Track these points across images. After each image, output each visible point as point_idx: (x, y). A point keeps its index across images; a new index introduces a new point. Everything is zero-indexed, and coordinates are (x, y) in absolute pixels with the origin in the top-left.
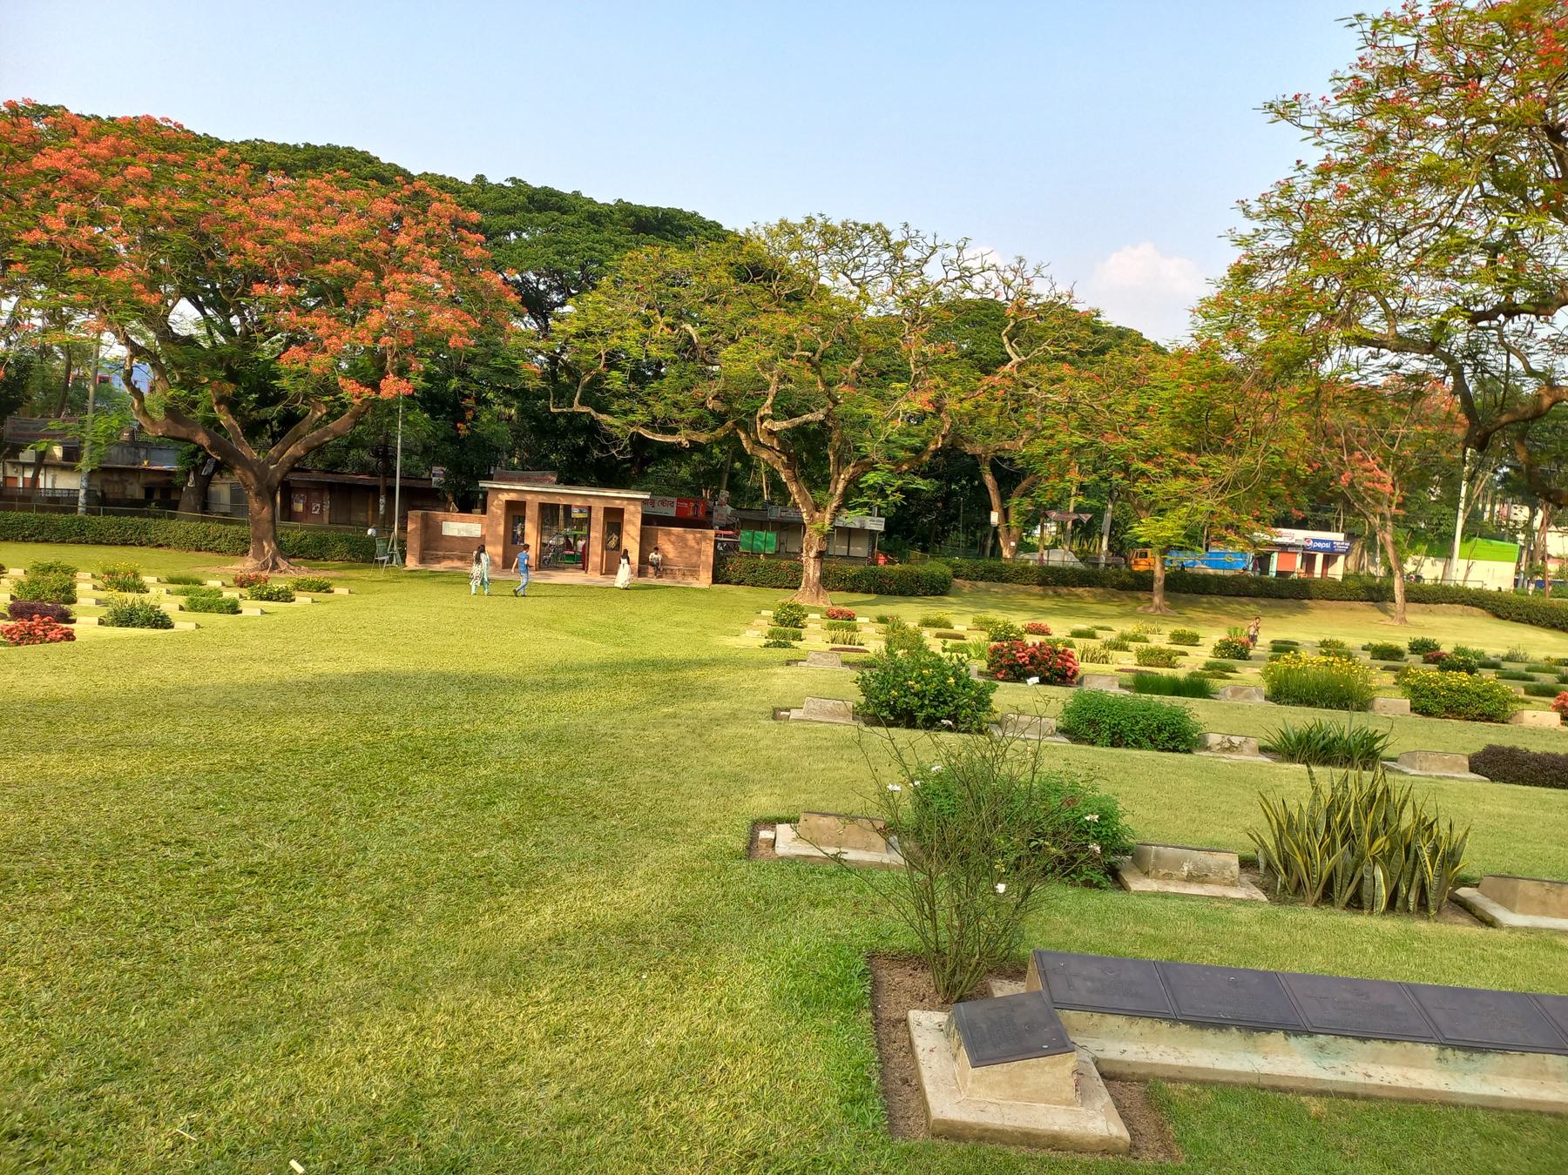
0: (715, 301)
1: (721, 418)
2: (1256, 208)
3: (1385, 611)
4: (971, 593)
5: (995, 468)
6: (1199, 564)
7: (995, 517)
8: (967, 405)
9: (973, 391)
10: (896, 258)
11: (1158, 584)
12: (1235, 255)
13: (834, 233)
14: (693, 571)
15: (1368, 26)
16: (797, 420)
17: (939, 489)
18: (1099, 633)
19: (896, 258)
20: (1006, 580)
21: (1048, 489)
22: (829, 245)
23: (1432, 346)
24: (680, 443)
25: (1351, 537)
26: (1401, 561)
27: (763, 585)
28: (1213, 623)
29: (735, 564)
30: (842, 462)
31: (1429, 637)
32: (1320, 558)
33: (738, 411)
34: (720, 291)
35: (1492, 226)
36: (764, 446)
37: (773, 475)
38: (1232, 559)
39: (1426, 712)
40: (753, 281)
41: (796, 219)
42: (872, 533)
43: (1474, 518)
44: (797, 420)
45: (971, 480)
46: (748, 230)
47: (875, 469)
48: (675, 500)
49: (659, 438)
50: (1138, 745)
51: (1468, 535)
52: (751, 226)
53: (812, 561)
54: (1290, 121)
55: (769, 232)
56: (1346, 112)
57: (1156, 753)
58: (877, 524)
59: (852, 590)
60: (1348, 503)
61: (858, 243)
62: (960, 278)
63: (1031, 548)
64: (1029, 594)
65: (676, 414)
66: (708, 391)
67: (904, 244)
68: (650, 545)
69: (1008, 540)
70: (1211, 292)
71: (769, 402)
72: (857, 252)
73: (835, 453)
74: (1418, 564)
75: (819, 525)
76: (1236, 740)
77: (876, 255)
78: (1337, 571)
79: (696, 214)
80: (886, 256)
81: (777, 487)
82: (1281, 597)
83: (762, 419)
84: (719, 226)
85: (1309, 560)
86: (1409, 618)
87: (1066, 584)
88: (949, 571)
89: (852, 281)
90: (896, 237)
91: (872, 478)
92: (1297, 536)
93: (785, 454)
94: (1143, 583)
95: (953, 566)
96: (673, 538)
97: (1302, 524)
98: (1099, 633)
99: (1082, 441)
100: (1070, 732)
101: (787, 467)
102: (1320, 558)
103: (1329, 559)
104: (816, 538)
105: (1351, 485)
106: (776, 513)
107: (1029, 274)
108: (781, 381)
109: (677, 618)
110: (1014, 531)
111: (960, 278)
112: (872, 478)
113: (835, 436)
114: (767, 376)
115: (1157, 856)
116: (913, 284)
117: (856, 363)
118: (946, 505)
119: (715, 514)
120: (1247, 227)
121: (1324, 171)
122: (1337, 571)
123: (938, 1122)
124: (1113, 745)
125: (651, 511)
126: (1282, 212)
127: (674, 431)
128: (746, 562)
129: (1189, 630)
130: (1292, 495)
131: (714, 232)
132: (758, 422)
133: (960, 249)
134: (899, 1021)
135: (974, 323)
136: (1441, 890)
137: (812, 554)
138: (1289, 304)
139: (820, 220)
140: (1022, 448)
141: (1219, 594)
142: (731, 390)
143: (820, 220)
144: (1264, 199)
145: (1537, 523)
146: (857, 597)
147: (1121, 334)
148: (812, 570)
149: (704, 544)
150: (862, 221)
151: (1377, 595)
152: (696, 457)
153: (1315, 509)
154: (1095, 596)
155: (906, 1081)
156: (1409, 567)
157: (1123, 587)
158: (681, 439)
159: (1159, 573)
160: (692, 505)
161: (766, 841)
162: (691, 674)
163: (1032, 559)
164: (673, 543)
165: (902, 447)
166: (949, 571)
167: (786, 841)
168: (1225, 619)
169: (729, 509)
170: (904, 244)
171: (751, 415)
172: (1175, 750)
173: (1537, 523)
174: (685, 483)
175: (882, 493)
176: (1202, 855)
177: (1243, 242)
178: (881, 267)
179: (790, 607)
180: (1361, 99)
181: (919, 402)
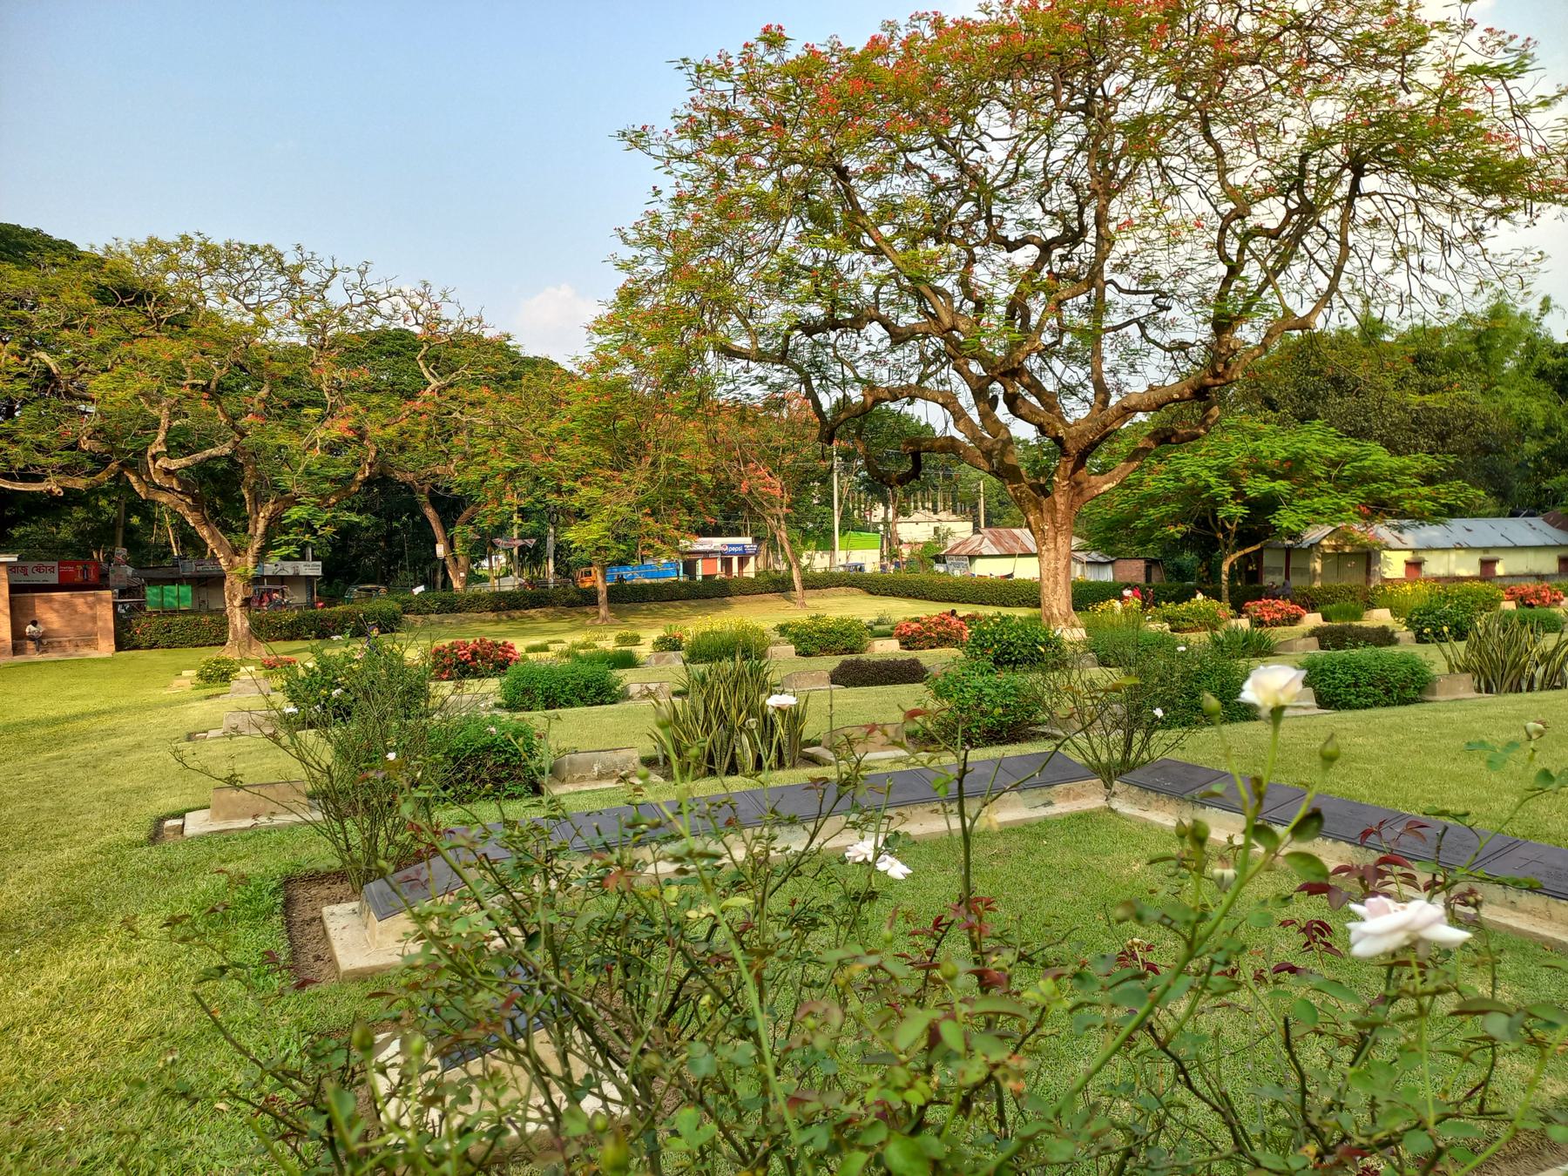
0: (76, 327)
1: (101, 461)
2: (632, 235)
3: (789, 599)
4: (424, 627)
5: (435, 501)
6: (635, 576)
7: (440, 550)
8: (391, 431)
9: (396, 416)
10: (294, 282)
11: (602, 597)
12: (622, 278)
13: (216, 250)
14: (89, 640)
15: (692, 70)
16: (199, 456)
17: (377, 526)
18: (551, 646)
19: (294, 282)
20: (459, 610)
21: (487, 518)
22: (212, 267)
23: (783, 356)
24: (50, 492)
25: (757, 540)
26: (798, 557)
27: (182, 645)
28: (651, 626)
29: (142, 626)
30: (259, 500)
31: (822, 613)
32: (735, 560)
33: (123, 451)
34: (81, 314)
35: (816, 258)
36: (160, 488)
37: (181, 525)
38: (662, 568)
39: (806, 654)
40: (122, 305)
41: (169, 236)
42: (309, 579)
43: (846, 515)
44: (199, 456)
45: (411, 517)
46: (108, 248)
47: (299, 504)
48: (55, 564)
49: (19, 486)
50: (570, 704)
51: (844, 530)
52: (112, 243)
53: (238, 611)
54: (642, 148)
55: (136, 251)
56: (686, 146)
57: (585, 709)
58: (312, 569)
59: (291, 639)
60: (751, 510)
61: (247, 265)
62: (366, 303)
63: (483, 579)
64: (484, 621)
65: (41, 459)
66: (82, 429)
67: (300, 268)
68: (26, 615)
69: (457, 569)
70: (606, 311)
71: (161, 437)
72: (247, 276)
73: (250, 491)
74: (811, 558)
75: (241, 570)
76: (652, 687)
77: (271, 279)
78: (750, 570)
79: (39, 231)
80: (282, 280)
81: (190, 540)
82: (708, 597)
83: (155, 458)
84: (72, 247)
85: (727, 563)
86: (808, 602)
87: (517, 608)
88: (397, 607)
89: (246, 306)
90: (290, 260)
91: (295, 513)
92: (716, 543)
93: (187, 495)
94: (589, 598)
95: (402, 602)
96: (56, 606)
97: (717, 532)
98: (551, 646)
99: (514, 465)
100: (511, 706)
101: (193, 509)
102: (735, 560)
103: (743, 562)
104: (239, 584)
105: (750, 492)
106: (191, 567)
107: (436, 299)
108: (175, 415)
109: (71, 692)
110: (462, 560)
111: (366, 303)
112: (295, 513)
113: (247, 473)
114: (155, 412)
115: (571, 763)
116: (315, 308)
117: (263, 393)
118: (389, 543)
119: (111, 576)
120: (628, 253)
121: (679, 201)
122: (750, 570)
123: (347, 973)
124: (547, 708)
125: (22, 579)
126: (653, 241)
127: (38, 479)
128: (157, 622)
129: (630, 633)
130: (704, 505)
131: (67, 248)
132: (150, 461)
133: (362, 273)
134: (314, 919)
135: (390, 354)
136: (792, 746)
137: (237, 602)
138: (666, 319)
139: (197, 239)
140: (456, 475)
141: (656, 600)
142: (110, 426)
143: (197, 239)
144: (637, 227)
145: (890, 516)
146: (297, 645)
147: (533, 363)
148: (239, 620)
149: (101, 609)
150: (249, 242)
151: (780, 586)
152: (79, 513)
153: (727, 518)
154: (547, 615)
155: (317, 958)
156: (804, 561)
157: (572, 604)
158: (52, 485)
159: (601, 586)
160: (80, 567)
161: (174, 829)
162: (85, 723)
163: (484, 589)
164: (57, 611)
165: (326, 479)
166: (397, 607)
167: (196, 824)
168: (662, 621)
169: (130, 571)
170: (300, 268)
171: (141, 454)
172: (602, 703)
173: (890, 516)
174: (67, 546)
175: (308, 526)
176: (608, 754)
177: (625, 266)
178: (278, 292)
179: (217, 662)
180: (696, 135)
181: (336, 429)
